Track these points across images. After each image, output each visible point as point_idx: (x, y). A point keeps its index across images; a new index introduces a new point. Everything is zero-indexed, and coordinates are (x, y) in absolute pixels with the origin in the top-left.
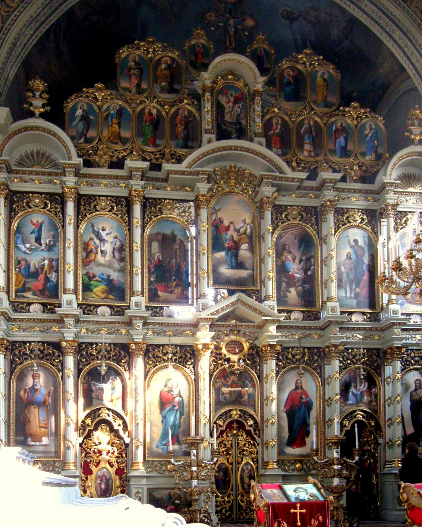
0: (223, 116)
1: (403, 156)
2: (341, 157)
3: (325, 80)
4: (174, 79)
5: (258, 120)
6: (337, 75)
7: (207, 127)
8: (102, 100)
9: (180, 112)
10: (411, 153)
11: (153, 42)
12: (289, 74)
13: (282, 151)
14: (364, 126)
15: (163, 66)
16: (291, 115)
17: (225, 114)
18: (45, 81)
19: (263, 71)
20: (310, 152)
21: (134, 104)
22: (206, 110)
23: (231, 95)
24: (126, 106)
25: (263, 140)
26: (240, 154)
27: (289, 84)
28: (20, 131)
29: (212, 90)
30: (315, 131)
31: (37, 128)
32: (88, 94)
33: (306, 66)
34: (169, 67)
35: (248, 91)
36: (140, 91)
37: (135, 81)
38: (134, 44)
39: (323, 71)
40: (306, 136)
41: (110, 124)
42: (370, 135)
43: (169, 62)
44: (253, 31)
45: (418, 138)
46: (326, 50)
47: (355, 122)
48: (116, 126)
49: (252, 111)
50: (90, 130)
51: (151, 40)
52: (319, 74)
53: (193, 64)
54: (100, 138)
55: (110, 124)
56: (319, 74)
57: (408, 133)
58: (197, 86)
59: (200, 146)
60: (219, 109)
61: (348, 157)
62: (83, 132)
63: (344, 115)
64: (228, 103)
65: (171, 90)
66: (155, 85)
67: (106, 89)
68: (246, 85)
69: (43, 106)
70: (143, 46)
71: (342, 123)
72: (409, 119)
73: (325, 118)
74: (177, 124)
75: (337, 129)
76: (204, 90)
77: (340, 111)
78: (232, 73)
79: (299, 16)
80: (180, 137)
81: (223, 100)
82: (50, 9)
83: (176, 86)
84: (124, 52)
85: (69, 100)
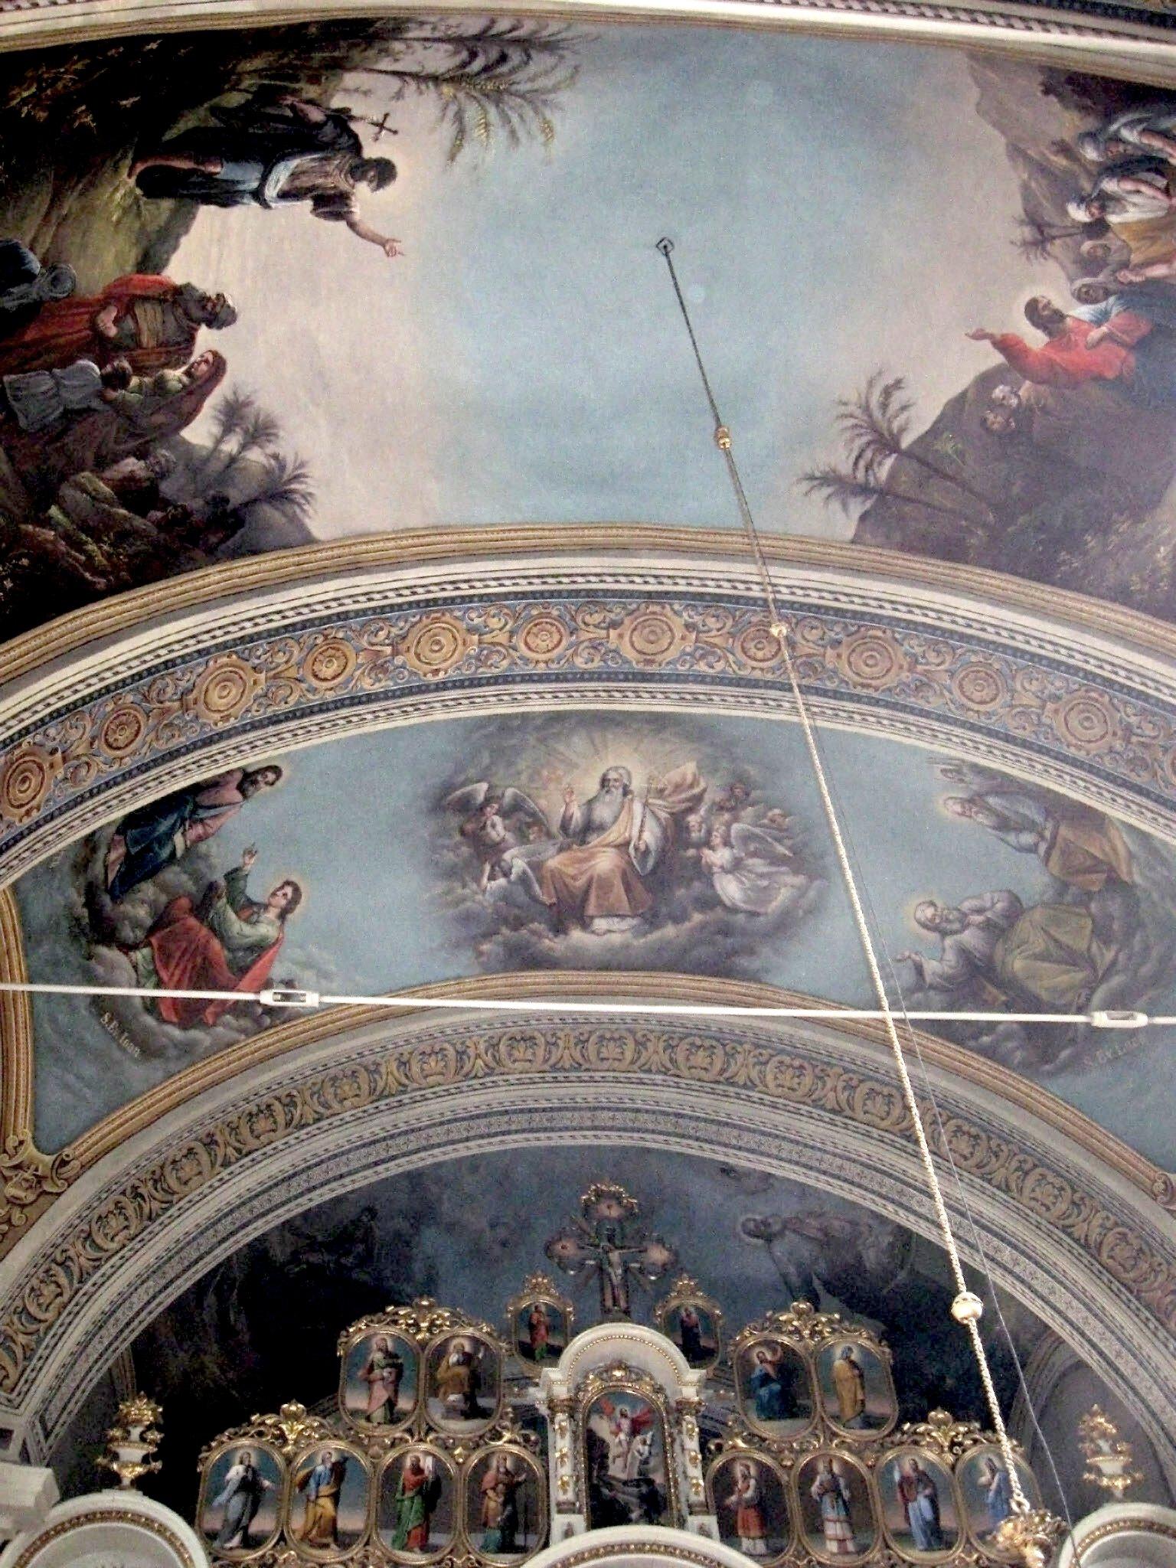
0: (604, 1467)
1: (1093, 1533)
2: (929, 1548)
3: (853, 1364)
4: (477, 1390)
5: (695, 1472)
6: (884, 1353)
7: (562, 1497)
8: (296, 1442)
9: (494, 1463)
10: (1111, 1524)
11: (429, 1308)
12: (762, 1361)
13: (767, 1546)
14: (972, 1466)
15: (453, 1358)
16: (781, 1451)
17: (610, 1461)
18: (158, 1403)
19: (695, 1353)
20: (841, 1541)
21: (376, 1448)
22: (557, 1455)
23: (624, 1415)
24: (357, 1453)
25: (711, 1521)
26: (653, 1561)
27: (765, 1379)
28: (76, 1521)
29: (571, 1407)
30: (848, 1487)
31: (121, 1515)
32: (262, 1428)
33: (802, 1338)
34: (467, 1359)
35: (666, 1402)
36: (393, 1416)
37: (381, 1394)
38: (385, 1313)
39: (847, 1344)
40: (827, 1500)
41: (313, 1498)
42: (994, 1486)
43: (468, 1349)
44: (669, 1271)
45: (1119, 1483)
46: (850, 1291)
47: (950, 1458)
48: (327, 1504)
49: (677, 1447)
50: (260, 1511)
51: (425, 1303)
52: (838, 1352)
53: (527, 1351)
54: (282, 1534)
55: (313, 1498)
56: (838, 1352)
57: (1090, 1472)
58: (536, 1396)
59: (546, 1545)
60: (594, 1451)
61: (949, 1546)
62: (239, 1520)
63: (916, 1443)
64: (616, 1435)
65: (472, 1411)
66: (432, 1401)
67: (308, 1413)
68: (659, 1390)
69: (146, 1460)
70: (407, 1316)
71: (916, 1463)
72: (1082, 1440)
73: (868, 1453)
74: (485, 1493)
75: (905, 1479)
76: (552, 1406)
77: (903, 1433)
78: (621, 1365)
79: (785, 1227)
80: (492, 1524)
81: (602, 1427)
82: (147, 1292)
83: (483, 1402)
84: (358, 1332)
85: (213, 1444)
